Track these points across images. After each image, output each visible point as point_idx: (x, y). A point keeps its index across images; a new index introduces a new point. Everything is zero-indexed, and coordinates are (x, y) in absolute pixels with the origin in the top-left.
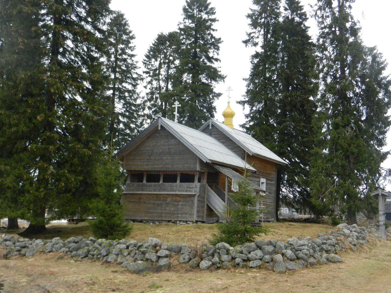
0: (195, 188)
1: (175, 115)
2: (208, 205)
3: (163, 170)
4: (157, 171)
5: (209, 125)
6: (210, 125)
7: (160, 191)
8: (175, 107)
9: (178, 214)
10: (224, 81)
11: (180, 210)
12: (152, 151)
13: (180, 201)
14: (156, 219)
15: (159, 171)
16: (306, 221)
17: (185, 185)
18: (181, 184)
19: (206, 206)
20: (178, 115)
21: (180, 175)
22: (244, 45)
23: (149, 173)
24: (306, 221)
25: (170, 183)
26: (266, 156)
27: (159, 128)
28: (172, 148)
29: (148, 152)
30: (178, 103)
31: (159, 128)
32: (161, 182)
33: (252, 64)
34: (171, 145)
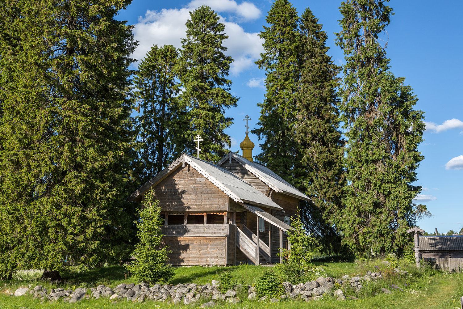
0: (223, 229)
2: (237, 247)
5: (229, 159)
6: (230, 160)
19: (235, 249)
20: (196, 148)
26: (291, 192)
29: (171, 192)
30: (200, 137)
33: (422, 132)
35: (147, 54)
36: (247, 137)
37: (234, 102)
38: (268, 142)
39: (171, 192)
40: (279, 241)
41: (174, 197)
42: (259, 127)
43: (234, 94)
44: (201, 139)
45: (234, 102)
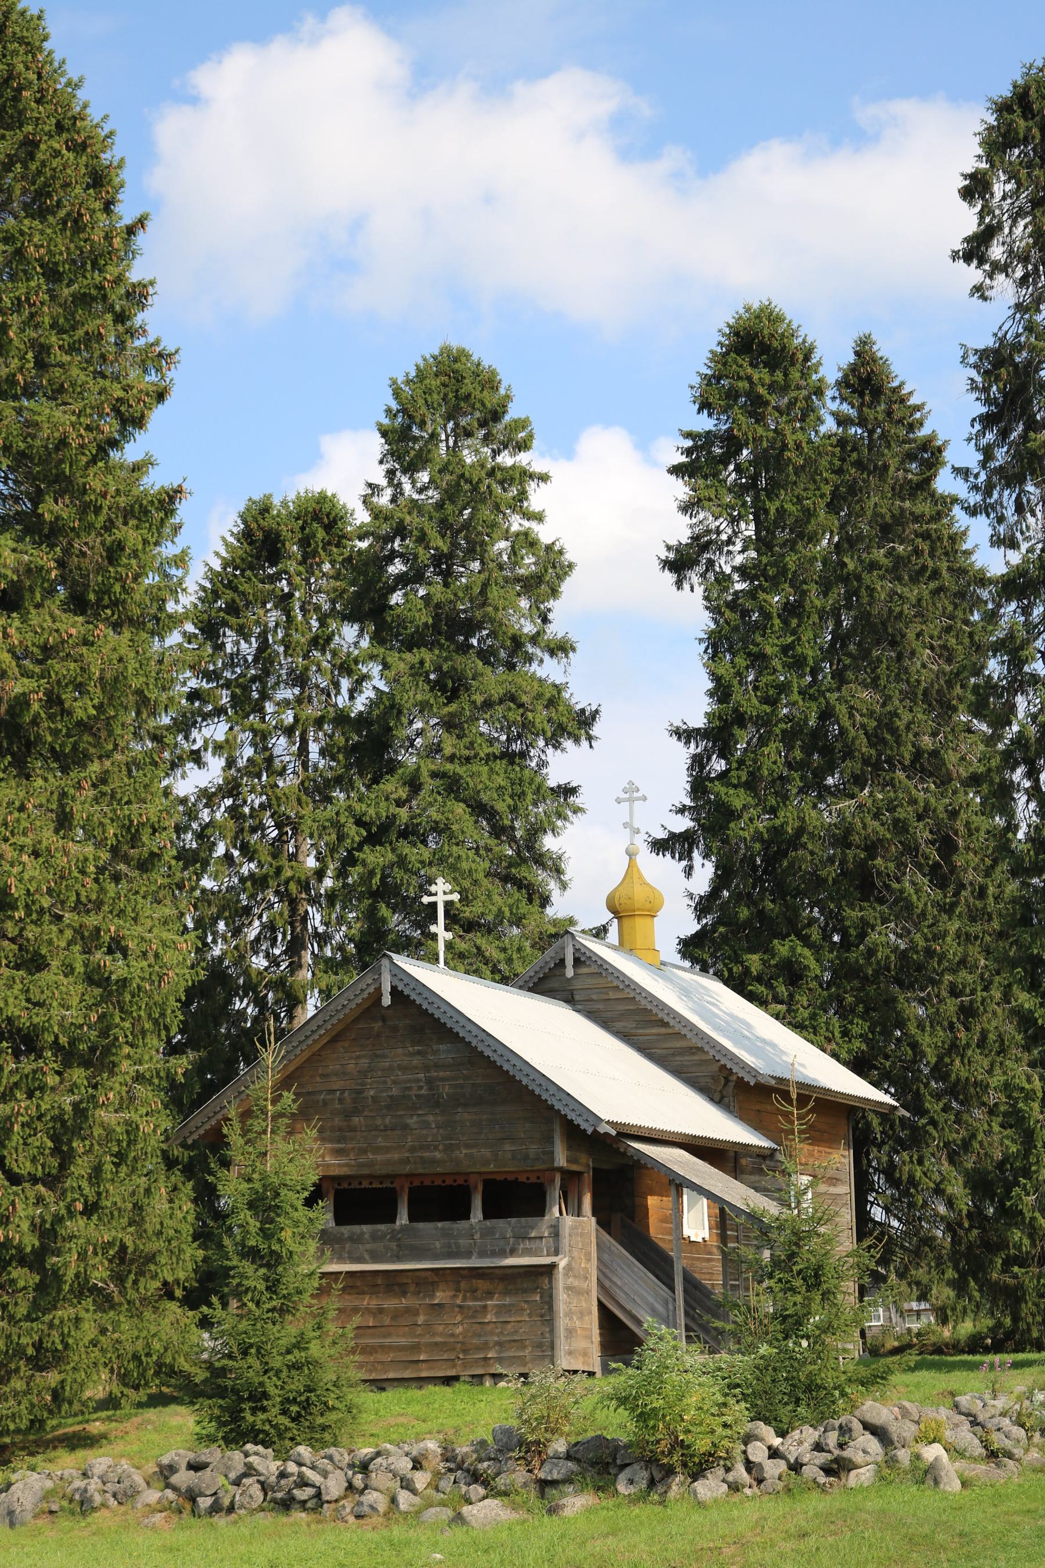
1: (434, 937)
3: (408, 1169)
4: (381, 1178)
5: (562, 961)
7: (399, 1259)
8: (433, 905)
9: (485, 1347)
10: (590, 738)
11: (492, 1333)
12: (359, 1092)
13: (490, 1294)
14: (391, 1375)
15: (392, 1177)
16: (974, 1345)
17: (506, 1226)
18: (488, 1223)
20: (433, 929)
21: (480, 1188)
22: (670, 577)
23: (345, 1185)
24: (974, 1345)
25: (440, 1225)
27: (387, 1000)
28: (442, 1079)
29: (341, 1100)
30: (448, 887)
31: (387, 1000)
32: (403, 1219)
34: (437, 1066)
35: (224, 539)
36: (632, 865)
37: (580, 724)
38: (720, 881)
39: (341, 1100)
40: (393, 1262)
41: (356, 1120)
42: (683, 824)
43: (579, 697)
44: (451, 892)
45: (580, 724)
